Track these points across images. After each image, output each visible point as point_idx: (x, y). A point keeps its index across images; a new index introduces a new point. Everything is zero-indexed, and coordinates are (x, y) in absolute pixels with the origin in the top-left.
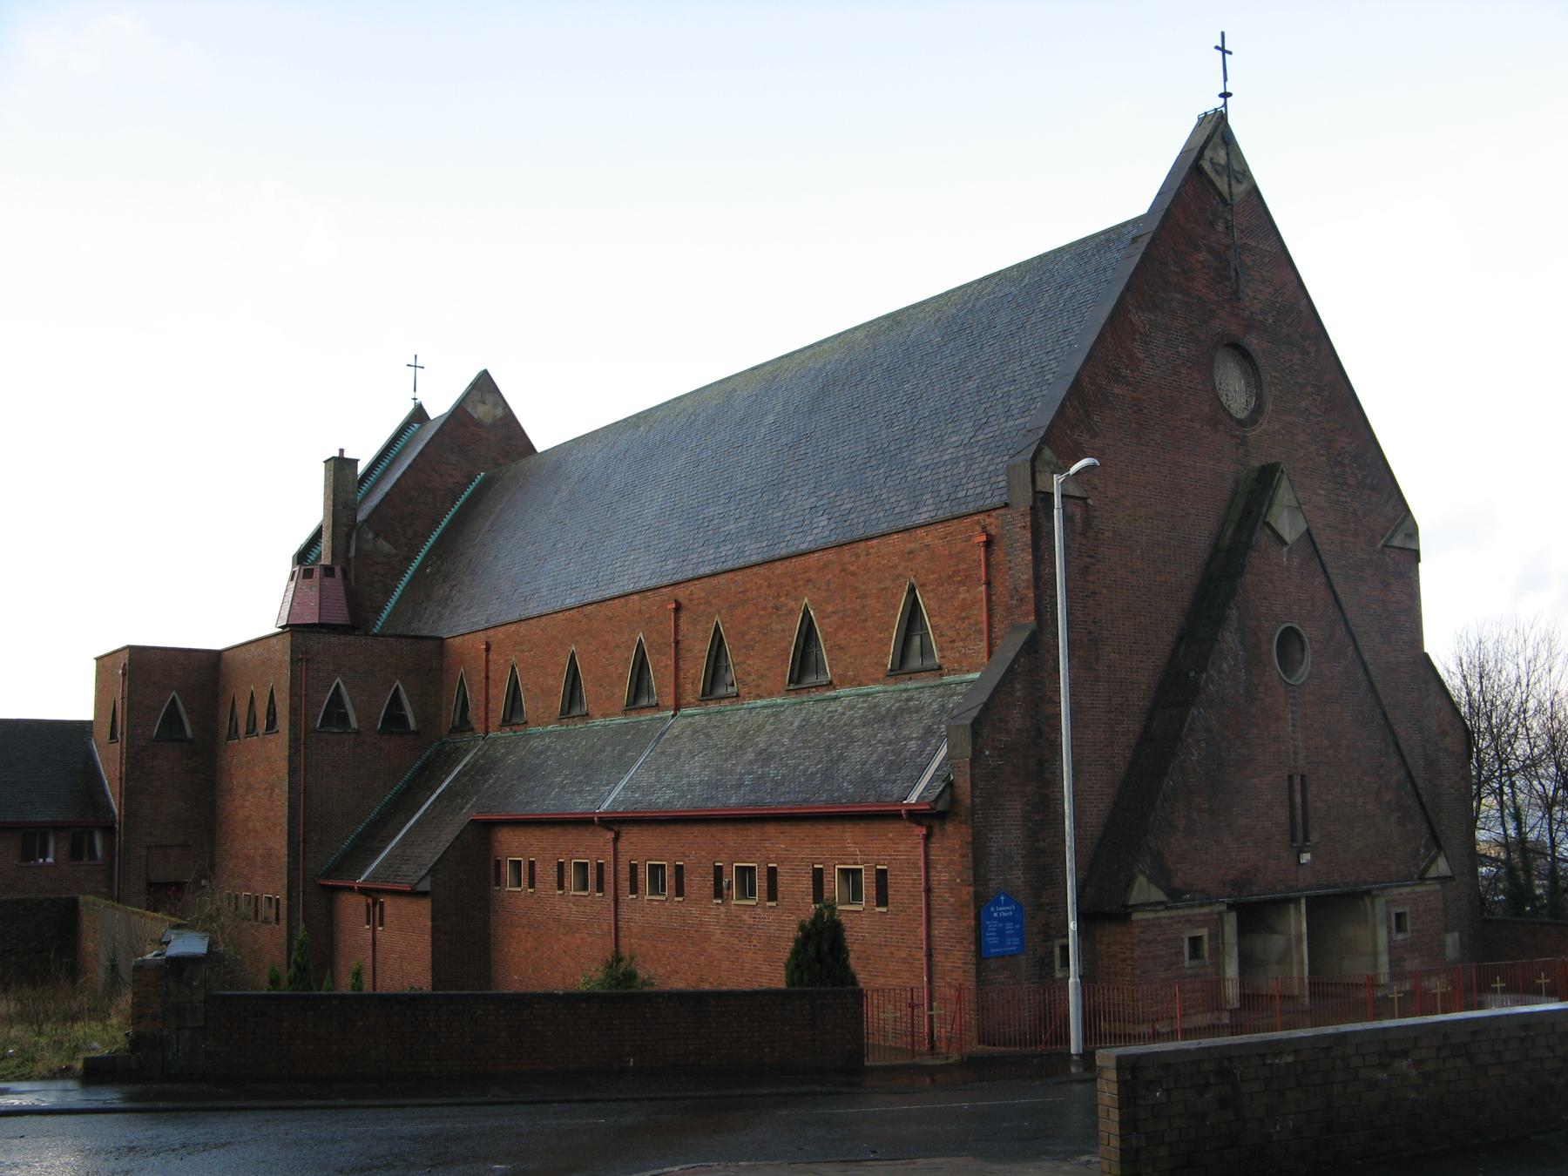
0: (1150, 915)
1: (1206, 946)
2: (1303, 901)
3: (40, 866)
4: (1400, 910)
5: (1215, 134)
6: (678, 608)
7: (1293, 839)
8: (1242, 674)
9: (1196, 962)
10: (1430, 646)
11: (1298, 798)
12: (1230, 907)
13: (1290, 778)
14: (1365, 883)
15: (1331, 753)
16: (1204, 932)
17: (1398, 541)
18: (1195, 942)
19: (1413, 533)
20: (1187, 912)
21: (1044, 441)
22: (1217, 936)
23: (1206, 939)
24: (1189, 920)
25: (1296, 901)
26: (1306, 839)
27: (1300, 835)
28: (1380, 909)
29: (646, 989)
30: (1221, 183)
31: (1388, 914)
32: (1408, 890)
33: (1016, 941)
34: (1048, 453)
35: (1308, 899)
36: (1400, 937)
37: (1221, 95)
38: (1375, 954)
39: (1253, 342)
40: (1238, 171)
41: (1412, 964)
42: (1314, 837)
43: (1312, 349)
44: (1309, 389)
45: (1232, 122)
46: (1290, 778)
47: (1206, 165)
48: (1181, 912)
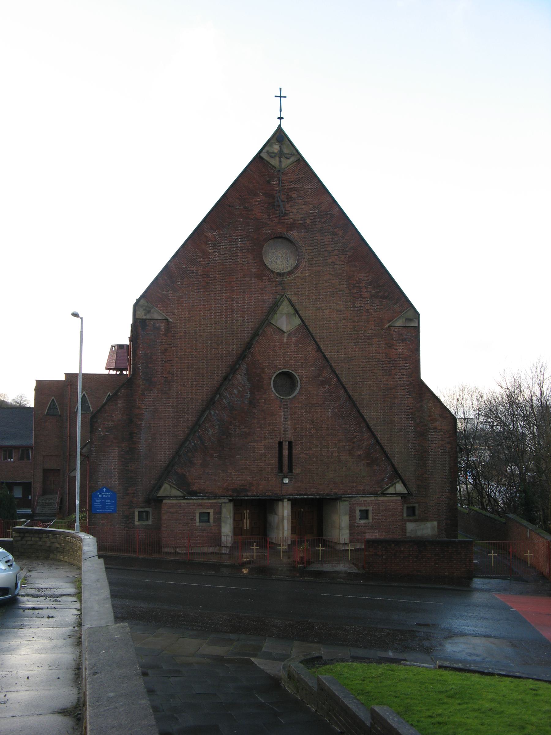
0: (174, 501)
1: (212, 517)
3: (9, 462)
5: (280, 136)
7: (281, 469)
8: (248, 395)
10: (424, 377)
11: (286, 452)
13: (280, 444)
14: (336, 494)
20: (200, 501)
22: (219, 514)
24: (200, 505)
26: (291, 470)
27: (285, 469)
29: (436, 529)
32: (373, 499)
33: (112, 507)
35: (294, 503)
37: (282, 118)
39: (294, 234)
43: (340, 233)
44: (336, 252)
46: (280, 444)
48: (195, 501)
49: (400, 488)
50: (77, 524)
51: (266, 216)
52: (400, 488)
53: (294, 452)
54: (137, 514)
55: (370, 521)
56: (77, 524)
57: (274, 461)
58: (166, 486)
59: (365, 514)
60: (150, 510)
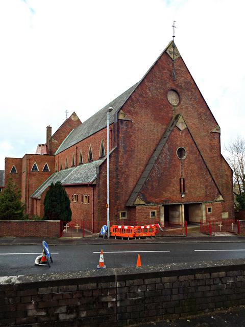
1: (156, 214)
2: (183, 206)
4: (209, 207)
5: (172, 45)
6: (77, 148)
7: (181, 192)
9: (153, 217)
11: (182, 183)
12: (163, 206)
13: (180, 179)
15: (192, 174)
16: (155, 211)
17: (214, 130)
18: (154, 213)
19: (219, 129)
21: (121, 108)
22: (159, 212)
23: (156, 212)
25: (181, 205)
26: (184, 191)
27: (182, 191)
28: (203, 207)
30: (172, 56)
31: (206, 208)
34: (121, 111)
35: (184, 205)
36: (209, 213)
38: (202, 216)
40: (176, 52)
41: (212, 219)
42: (186, 192)
45: (175, 42)
46: (180, 179)
47: (168, 52)
49: (221, 198)
50: (116, 277)
51: (168, 80)
52: (221, 198)
53: (185, 183)
54: (120, 214)
55: (150, 211)
56: (116, 277)
57: (178, 187)
58: (138, 199)
59: (210, 210)
60: (126, 211)
